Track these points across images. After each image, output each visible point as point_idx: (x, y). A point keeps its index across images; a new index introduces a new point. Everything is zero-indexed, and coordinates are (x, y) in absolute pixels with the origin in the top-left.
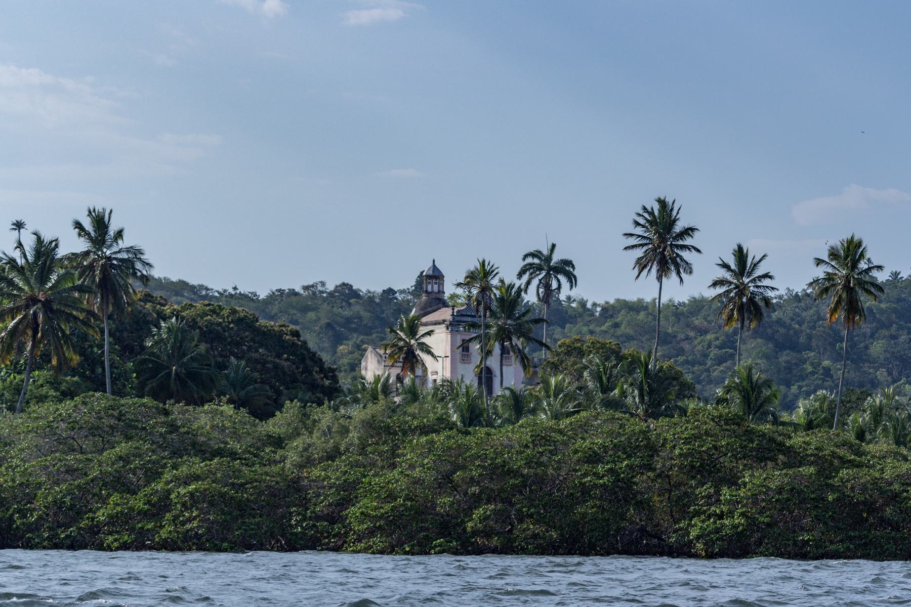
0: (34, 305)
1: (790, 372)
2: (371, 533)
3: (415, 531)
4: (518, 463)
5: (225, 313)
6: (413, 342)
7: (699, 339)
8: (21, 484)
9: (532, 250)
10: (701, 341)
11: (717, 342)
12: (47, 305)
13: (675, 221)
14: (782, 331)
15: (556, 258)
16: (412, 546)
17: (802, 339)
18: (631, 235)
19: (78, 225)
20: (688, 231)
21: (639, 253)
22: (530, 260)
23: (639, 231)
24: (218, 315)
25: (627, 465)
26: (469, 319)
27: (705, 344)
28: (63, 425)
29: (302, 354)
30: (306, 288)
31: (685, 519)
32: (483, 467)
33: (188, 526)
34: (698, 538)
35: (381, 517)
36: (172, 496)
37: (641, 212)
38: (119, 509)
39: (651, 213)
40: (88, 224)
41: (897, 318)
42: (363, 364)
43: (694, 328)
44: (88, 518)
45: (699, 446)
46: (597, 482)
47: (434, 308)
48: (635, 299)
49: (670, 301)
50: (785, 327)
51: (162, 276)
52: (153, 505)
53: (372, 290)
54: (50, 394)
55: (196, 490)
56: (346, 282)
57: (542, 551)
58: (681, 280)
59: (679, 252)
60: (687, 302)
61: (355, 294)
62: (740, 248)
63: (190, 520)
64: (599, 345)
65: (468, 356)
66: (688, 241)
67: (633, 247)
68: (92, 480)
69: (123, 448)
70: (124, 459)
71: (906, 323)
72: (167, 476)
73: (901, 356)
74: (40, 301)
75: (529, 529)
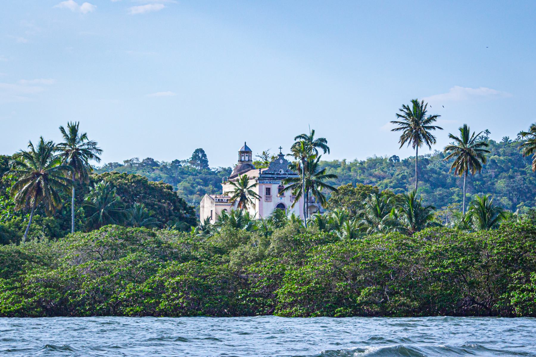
0: (38, 177)
1: (443, 201)
2: (292, 304)
3: (325, 301)
4: (390, 261)
5: (130, 177)
6: (245, 190)
7: (379, 183)
8: (72, 279)
10: (381, 184)
11: (392, 184)
12: (45, 177)
13: (424, 113)
14: (435, 176)
15: (315, 138)
16: (322, 312)
17: (449, 181)
18: (397, 122)
19: (62, 129)
20: (432, 118)
21: (401, 132)
23: (401, 120)
25: (463, 261)
26: (270, 176)
27: (384, 186)
29: (174, 199)
30: (126, 162)
31: (505, 292)
33: (177, 302)
34: (516, 304)
35: (300, 295)
36: (166, 284)
37: (402, 108)
39: (408, 109)
41: (512, 165)
42: (201, 204)
43: (375, 176)
44: (114, 298)
45: (510, 247)
46: (444, 271)
48: (333, 161)
49: (356, 160)
50: (436, 174)
53: (165, 161)
54: (36, 228)
55: (181, 280)
57: (408, 314)
58: (430, 147)
59: (426, 130)
60: (366, 161)
61: (155, 164)
62: (465, 127)
64: (364, 188)
65: (270, 197)
66: (433, 124)
68: (115, 276)
69: (131, 256)
70: (134, 263)
71: (519, 168)
72: (160, 272)
73: (518, 189)
74: (41, 174)
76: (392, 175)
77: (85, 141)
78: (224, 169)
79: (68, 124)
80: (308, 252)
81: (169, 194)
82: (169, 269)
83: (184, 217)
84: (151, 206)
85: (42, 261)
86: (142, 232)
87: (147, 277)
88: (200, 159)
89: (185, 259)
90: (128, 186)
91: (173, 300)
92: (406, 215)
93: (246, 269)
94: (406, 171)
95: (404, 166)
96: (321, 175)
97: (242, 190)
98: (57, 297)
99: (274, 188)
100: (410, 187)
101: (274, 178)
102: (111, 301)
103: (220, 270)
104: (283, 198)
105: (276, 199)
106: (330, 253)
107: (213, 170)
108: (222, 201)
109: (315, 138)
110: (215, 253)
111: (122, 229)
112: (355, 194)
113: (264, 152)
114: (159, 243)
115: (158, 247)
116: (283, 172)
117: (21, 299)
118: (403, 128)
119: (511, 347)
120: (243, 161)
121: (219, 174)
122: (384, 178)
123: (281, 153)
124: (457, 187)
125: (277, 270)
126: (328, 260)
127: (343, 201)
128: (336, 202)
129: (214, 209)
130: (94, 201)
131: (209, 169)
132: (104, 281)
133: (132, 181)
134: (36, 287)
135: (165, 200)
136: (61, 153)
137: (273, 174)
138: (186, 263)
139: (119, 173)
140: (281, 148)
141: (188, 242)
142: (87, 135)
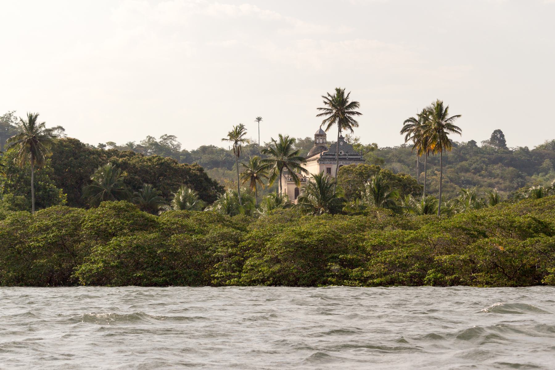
9: (406, 119)
22: (407, 124)
23: (327, 106)
26: (331, 157)
37: (327, 96)
59: (349, 115)
66: (356, 110)
67: (321, 115)
107: (511, 149)
116: (343, 153)
119: (335, 321)
137: (334, 155)
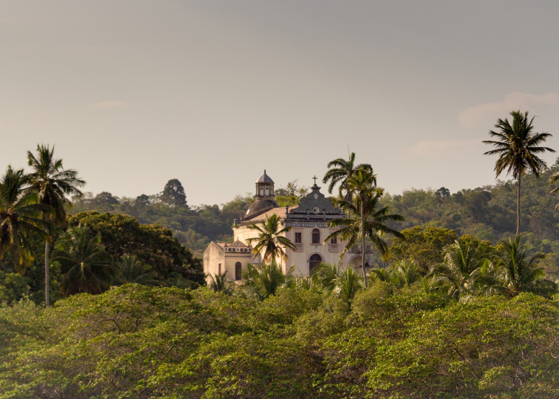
4: (523, 332)
9: (333, 160)
12: (14, 218)
13: (529, 128)
14: (499, 215)
15: (356, 164)
18: (490, 142)
20: (541, 137)
22: (333, 167)
23: (497, 139)
24: (108, 220)
26: (301, 216)
28: (108, 310)
29: (175, 249)
32: (493, 336)
33: (228, 389)
35: (399, 379)
36: (213, 364)
38: (168, 375)
39: (506, 124)
40: (37, 156)
44: (141, 383)
47: (267, 208)
51: (460, 189)
52: (197, 371)
53: (127, 197)
55: (233, 359)
56: (106, 191)
59: (532, 153)
63: (231, 383)
64: (437, 233)
66: (541, 144)
67: (493, 152)
68: (142, 353)
69: (161, 327)
72: (204, 348)
74: (9, 215)
75: (537, 388)
76: (440, 215)
77: (60, 170)
78: (208, 208)
79: (38, 147)
80: (406, 321)
81: (168, 242)
82: (215, 344)
83: (188, 274)
84: (146, 259)
85: (38, 334)
86: (173, 293)
87: (187, 355)
88: (174, 193)
89: (235, 330)
90: (112, 230)
91: (224, 386)
92: (506, 270)
93: (321, 344)
94: (459, 210)
95: (456, 202)
96: (381, 215)
97: (269, 236)
98: (63, 383)
99: (307, 233)
100: (465, 231)
101: (306, 219)
102: (137, 388)
103: (283, 345)
104: (319, 247)
105: (309, 249)
106: (439, 321)
107: (193, 209)
108: (234, 251)
109: (356, 164)
110: (272, 322)
111: (146, 289)
112: (425, 241)
113: (289, 184)
114: (197, 308)
115: (196, 313)
116: (318, 211)
117: (13, 385)
118: (499, 150)
120: (262, 196)
121: (201, 214)
122: (429, 219)
123: (315, 185)
124: (531, 231)
125: (364, 345)
126: (437, 332)
127: (408, 251)
128: (399, 252)
129: (223, 262)
130: (71, 251)
131: (187, 206)
132: (127, 361)
133: (118, 224)
134: (33, 369)
135: (163, 250)
136: (29, 186)
137: (306, 214)
138: (237, 336)
139: (98, 214)
140: (315, 178)
141: (233, 307)
142: (63, 162)
